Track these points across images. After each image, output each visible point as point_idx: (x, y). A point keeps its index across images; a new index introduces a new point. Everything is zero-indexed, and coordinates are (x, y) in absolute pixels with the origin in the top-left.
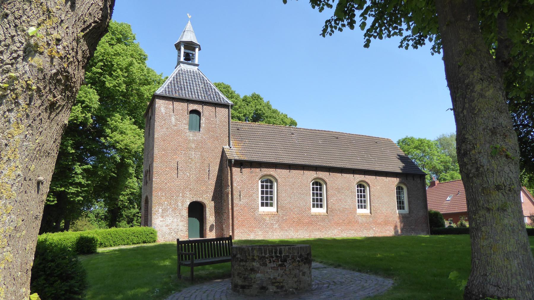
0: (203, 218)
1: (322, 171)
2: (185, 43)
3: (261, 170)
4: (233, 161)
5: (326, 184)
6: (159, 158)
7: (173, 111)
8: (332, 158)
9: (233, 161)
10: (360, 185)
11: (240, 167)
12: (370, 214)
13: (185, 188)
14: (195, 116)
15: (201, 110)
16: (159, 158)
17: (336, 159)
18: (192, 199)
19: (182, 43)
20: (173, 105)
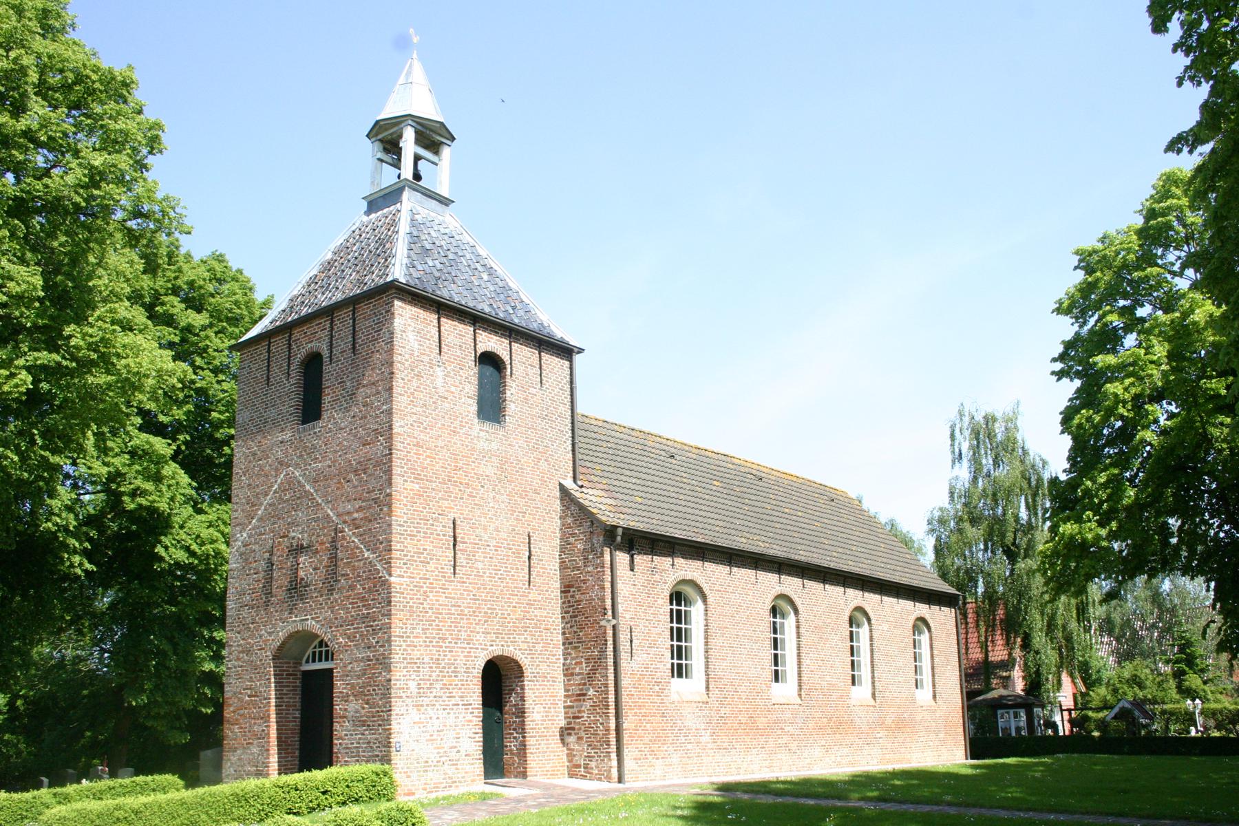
0: (301, 733)
1: (855, 587)
2: (418, 123)
3: (673, 565)
4: (620, 531)
5: (869, 620)
6: (406, 505)
7: (440, 347)
8: (791, 533)
9: (620, 531)
10: (677, 597)
11: (823, 583)
12: (872, 702)
13: (474, 612)
14: (489, 370)
15: (505, 357)
16: (406, 505)
17: (787, 533)
18: (490, 648)
19: (410, 122)
20: (439, 327)
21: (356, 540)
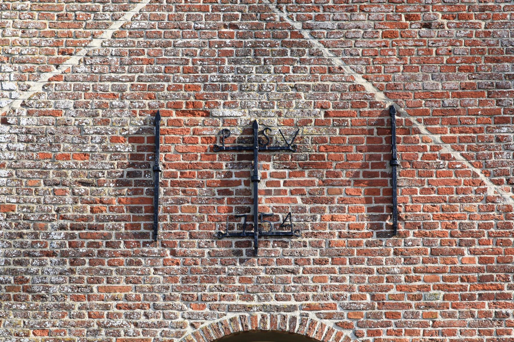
21: (457, 155)
